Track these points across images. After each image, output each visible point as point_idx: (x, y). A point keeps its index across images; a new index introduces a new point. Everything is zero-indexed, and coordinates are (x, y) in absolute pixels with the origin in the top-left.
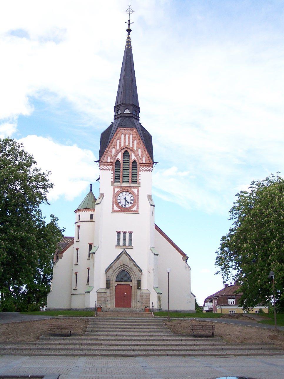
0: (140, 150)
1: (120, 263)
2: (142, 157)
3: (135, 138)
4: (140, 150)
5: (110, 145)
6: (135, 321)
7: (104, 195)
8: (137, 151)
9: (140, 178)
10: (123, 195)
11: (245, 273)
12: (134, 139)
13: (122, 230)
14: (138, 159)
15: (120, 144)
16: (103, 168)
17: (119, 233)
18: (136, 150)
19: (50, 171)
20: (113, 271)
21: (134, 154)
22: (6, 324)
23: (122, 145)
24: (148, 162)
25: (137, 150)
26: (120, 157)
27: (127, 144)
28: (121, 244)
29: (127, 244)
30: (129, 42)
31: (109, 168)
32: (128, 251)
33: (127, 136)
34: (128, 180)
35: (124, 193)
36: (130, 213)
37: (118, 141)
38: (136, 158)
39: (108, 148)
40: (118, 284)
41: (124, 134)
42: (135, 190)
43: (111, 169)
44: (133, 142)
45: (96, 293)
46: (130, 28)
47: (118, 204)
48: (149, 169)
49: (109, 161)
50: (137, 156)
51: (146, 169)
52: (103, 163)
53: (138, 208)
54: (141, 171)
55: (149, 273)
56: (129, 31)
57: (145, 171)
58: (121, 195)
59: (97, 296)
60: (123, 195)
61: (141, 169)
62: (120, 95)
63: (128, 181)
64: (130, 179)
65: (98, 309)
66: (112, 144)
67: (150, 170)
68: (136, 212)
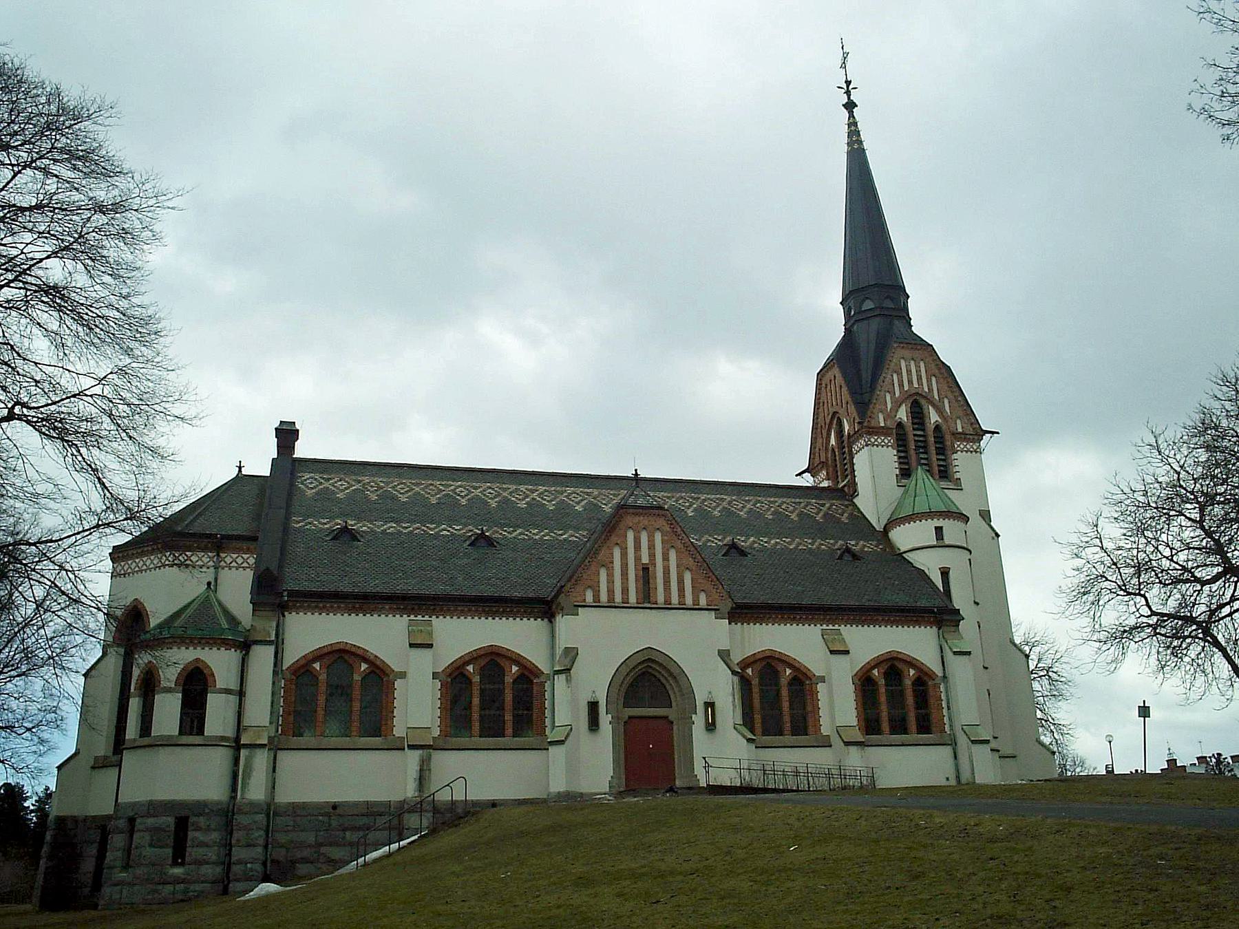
9: (957, 469)
11: (252, 804)
15: (901, 385)
22: (100, 124)
26: (903, 414)
30: (853, 124)
40: (631, 714)
50: (940, 411)
56: (850, 106)
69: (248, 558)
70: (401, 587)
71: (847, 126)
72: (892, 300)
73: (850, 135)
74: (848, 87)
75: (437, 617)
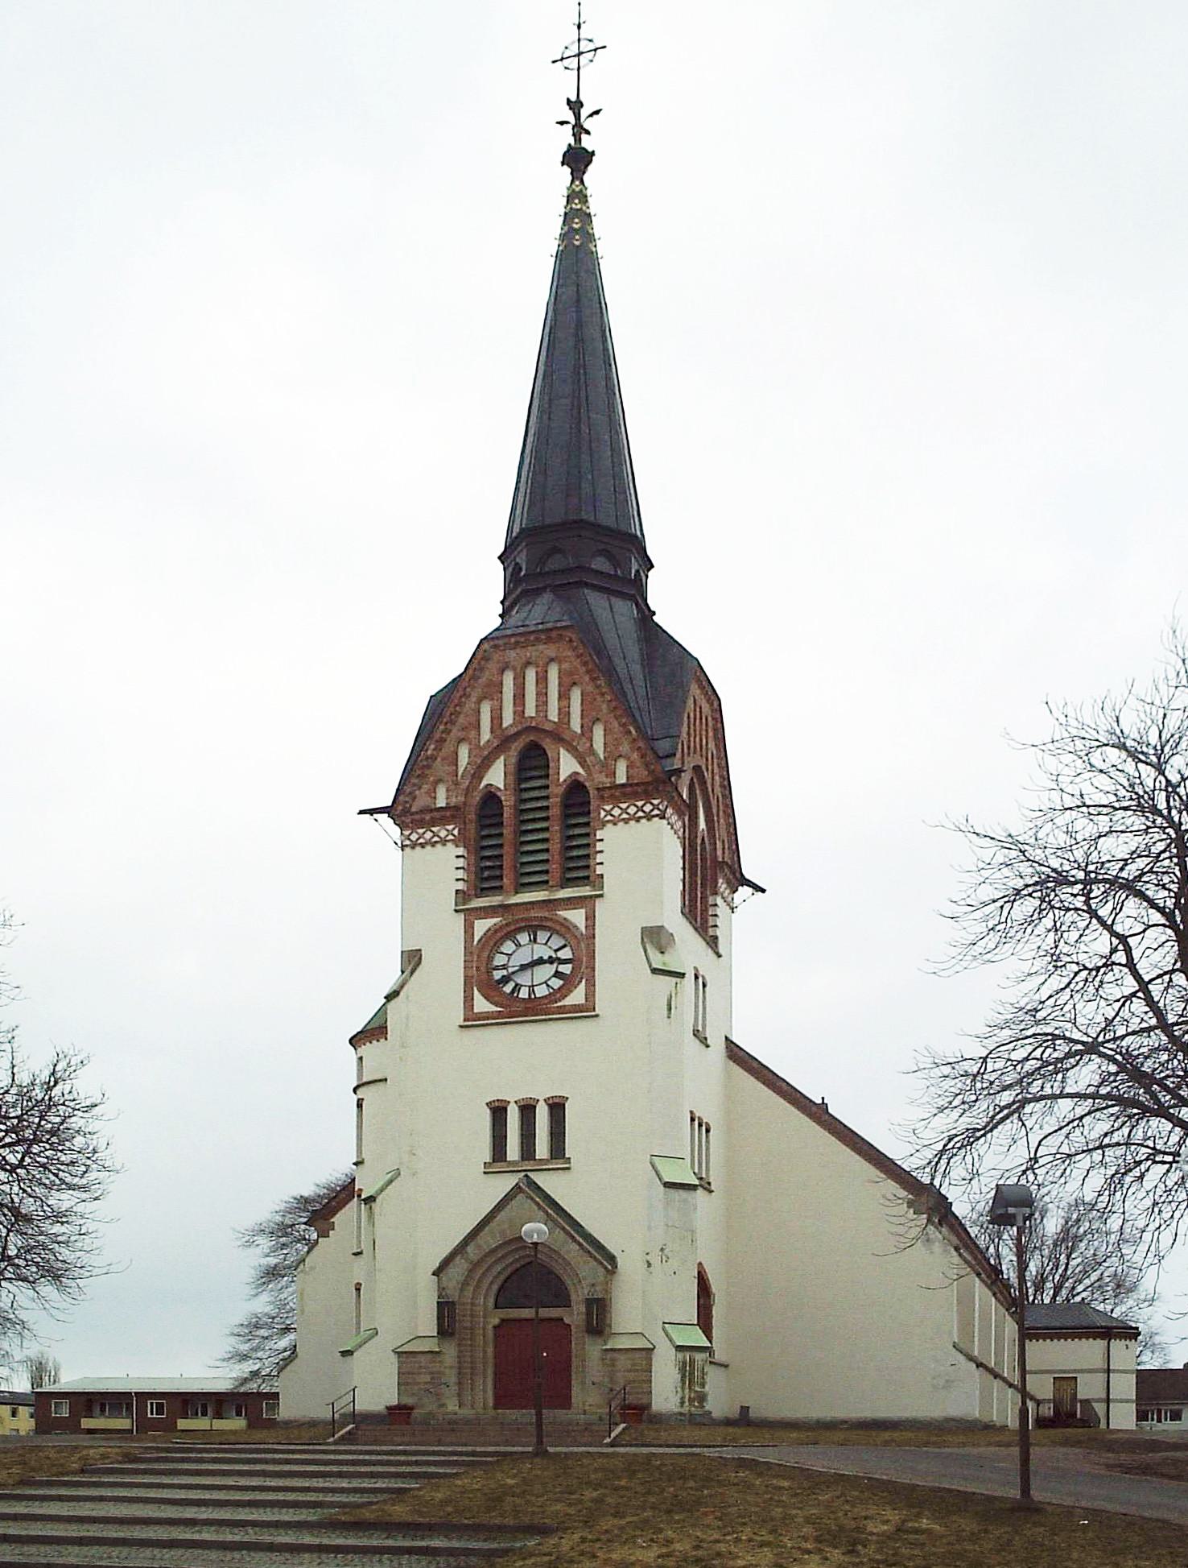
0: (598, 733)
1: (502, 1233)
2: (613, 756)
3: (571, 674)
4: (598, 733)
5: (442, 727)
6: (414, 1458)
7: (423, 953)
8: (583, 734)
10: (518, 945)
12: (566, 680)
13: (513, 1095)
14: (590, 774)
15: (497, 717)
16: (414, 837)
17: (498, 1112)
18: (579, 731)
19: (709, 1042)
20: (466, 1266)
21: (573, 750)
23: (508, 719)
24: (642, 774)
25: (587, 731)
27: (530, 710)
28: (513, 1151)
29: (542, 1149)
30: (577, 196)
31: (443, 834)
32: (548, 1182)
33: (531, 675)
34: (544, 878)
35: (523, 938)
36: (550, 1020)
37: (486, 710)
38: (581, 771)
39: (432, 747)
40: (502, 1316)
41: (514, 669)
42: (577, 917)
43: (451, 837)
44: (564, 696)
45: (394, 1359)
46: (587, 142)
47: (491, 989)
48: (648, 808)
49: (441, 802)
51: (632, 810)
52: (412, 814)
53: (590, 994)
54: (604, 824)
55: (649, 1265)
56: (577, 159)
57: (626, 821)
58: (508, 947)
59: (399, 1368)
60: (518, 945)
61: (603, 813)
62: (521, 498)
63: (547, 882)
64: (554, 867)
65: (398, 1414)
66: (453, 722)
67: (656, 812)
68: (586, 1011)
69: (439, 831)
70: (643, 953)
71: (565, 200)
72: (610, 557)
73: (567, 218)
74: (577, 116)
75: (378, 1041)
